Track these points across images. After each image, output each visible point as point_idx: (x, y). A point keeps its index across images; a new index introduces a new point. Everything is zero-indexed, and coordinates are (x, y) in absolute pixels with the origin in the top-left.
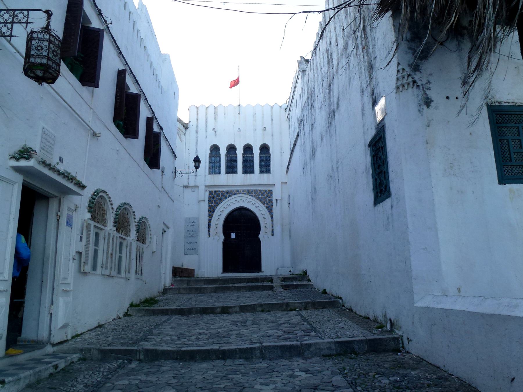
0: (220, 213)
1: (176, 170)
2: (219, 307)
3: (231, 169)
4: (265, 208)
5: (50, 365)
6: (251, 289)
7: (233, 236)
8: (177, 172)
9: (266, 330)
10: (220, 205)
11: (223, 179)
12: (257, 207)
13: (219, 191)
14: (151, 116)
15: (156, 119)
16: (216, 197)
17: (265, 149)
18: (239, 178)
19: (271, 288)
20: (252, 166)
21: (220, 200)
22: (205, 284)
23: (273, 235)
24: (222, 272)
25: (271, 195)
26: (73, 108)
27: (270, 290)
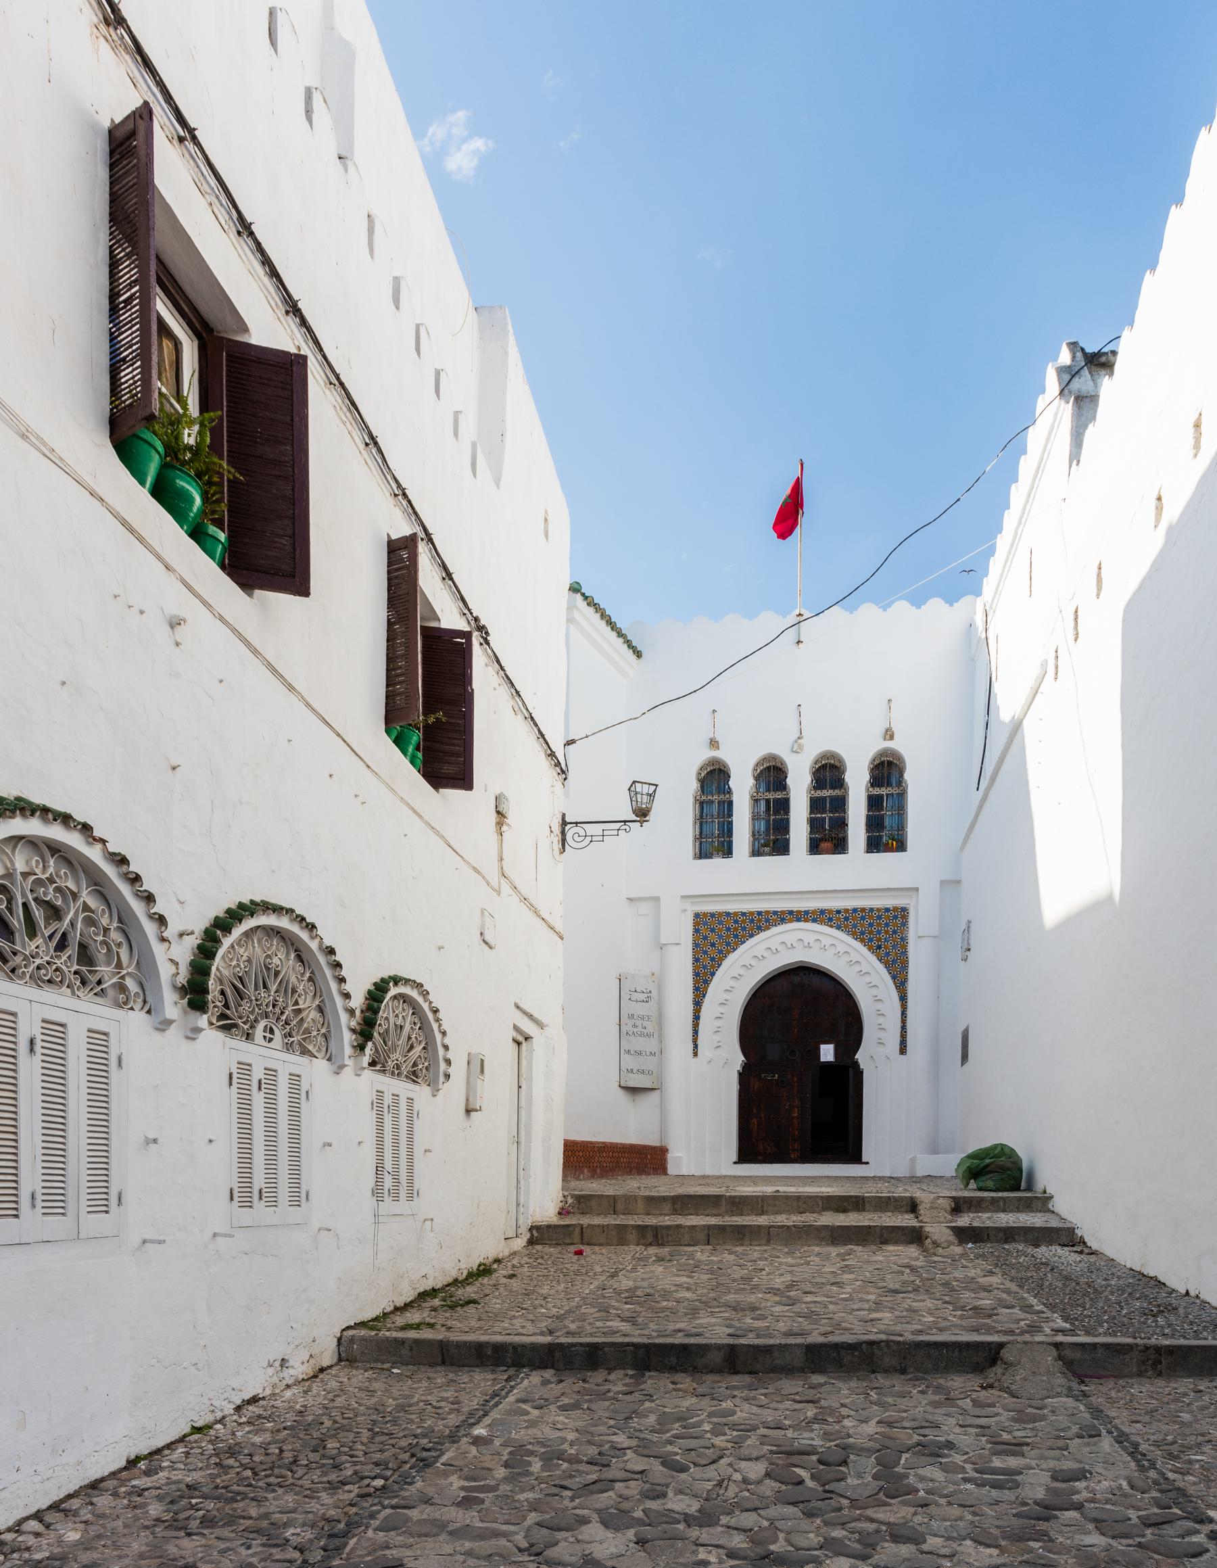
0: (733, 983)
1: (564, 823)
2: (719, 1347)
3: (773, 840)
4: (881, 968)
5: (84, 1519)
6: (838, 1236)
7: (827, 1053)
8: (571, 831)
9: (854, 1293)
10: (732, 957)
11: (744, 878)
12: (851, 963)
13: (728, 914)
14: (407, 531)
15: (188, 135)
16: (717, 935)
17: (887, 771)
18: (801, 874)
19: (916, 1237)
20: (841, 824)
22: (675, 1212)
23: (903, 1050)
24: (735, 1158)
25: (905, 924)
27: (911, 1242)
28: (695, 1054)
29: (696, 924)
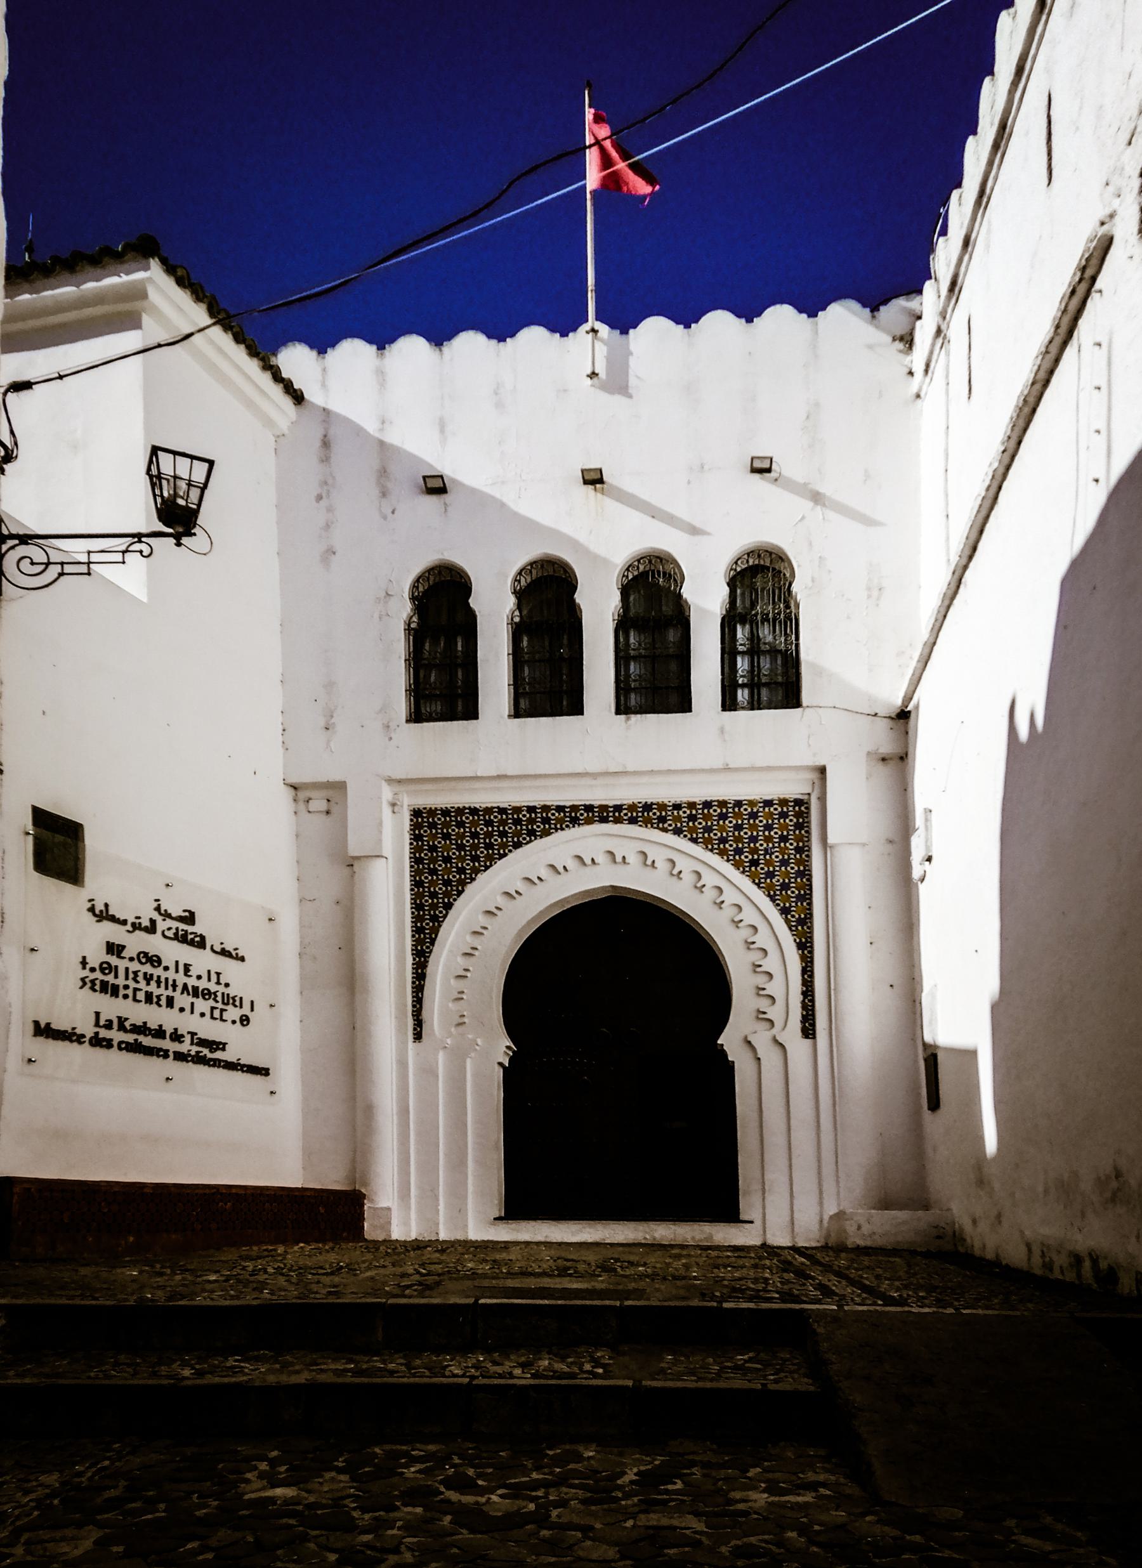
11: (499, 753)
16: (452, 846)
17: (761, 581)
18: (601, 748)
21: (482, 852)
26: (1114, 398)
28: (418, 1036)
29: (415, 826)
